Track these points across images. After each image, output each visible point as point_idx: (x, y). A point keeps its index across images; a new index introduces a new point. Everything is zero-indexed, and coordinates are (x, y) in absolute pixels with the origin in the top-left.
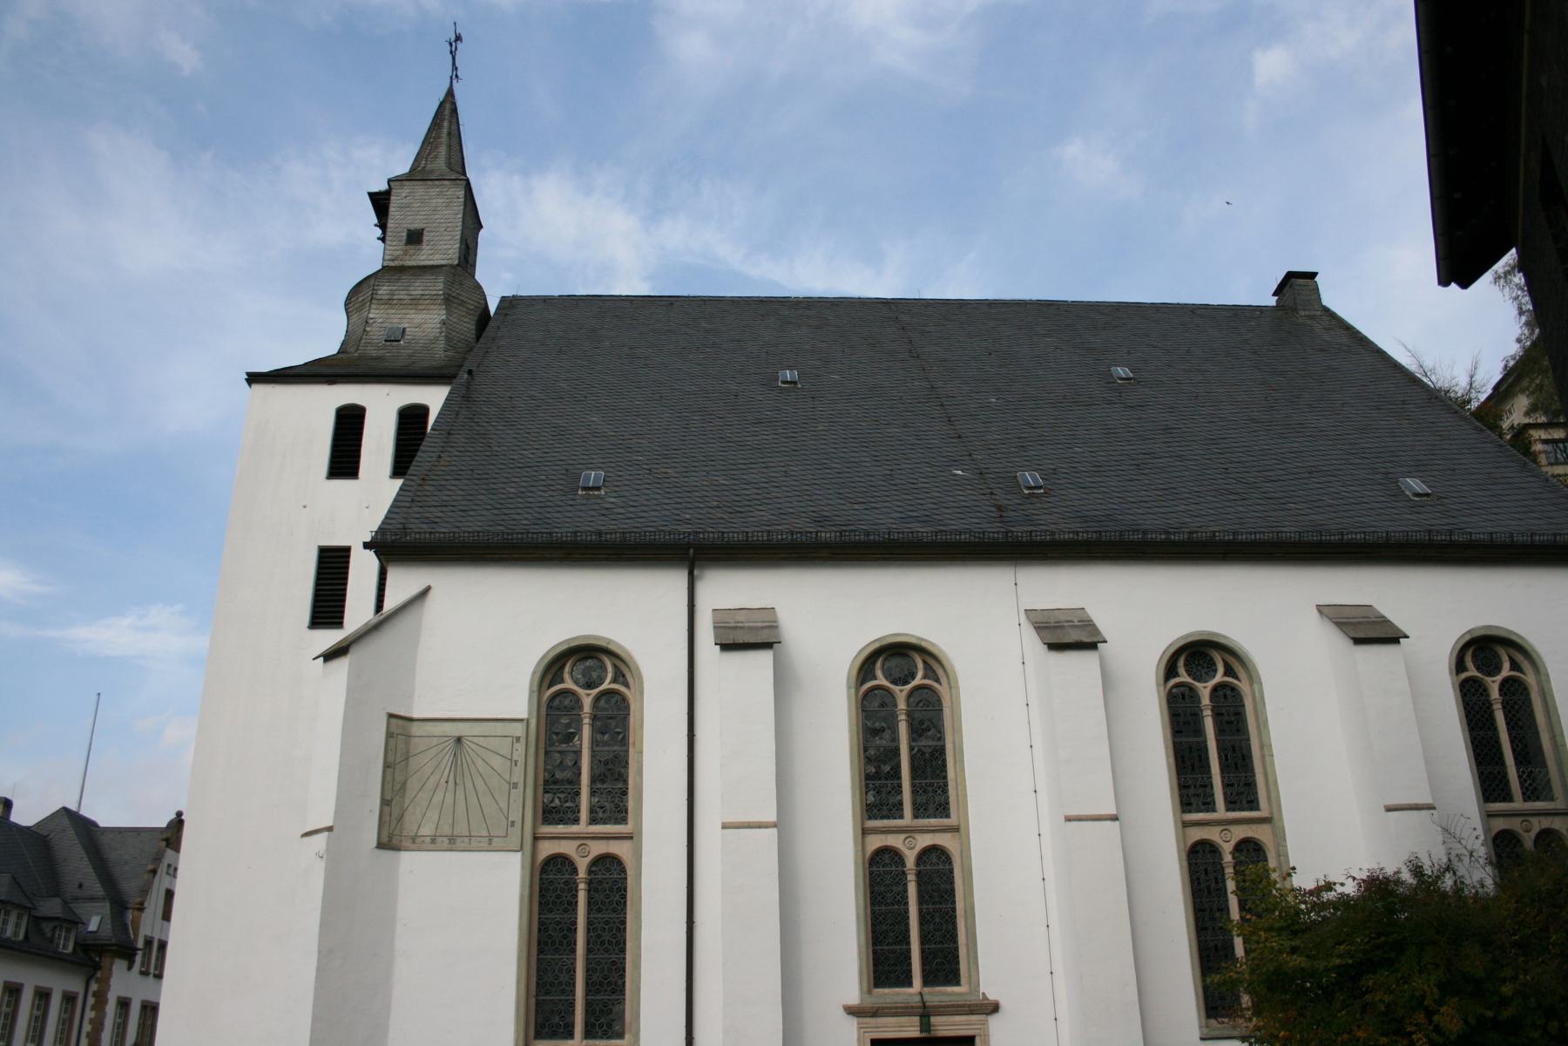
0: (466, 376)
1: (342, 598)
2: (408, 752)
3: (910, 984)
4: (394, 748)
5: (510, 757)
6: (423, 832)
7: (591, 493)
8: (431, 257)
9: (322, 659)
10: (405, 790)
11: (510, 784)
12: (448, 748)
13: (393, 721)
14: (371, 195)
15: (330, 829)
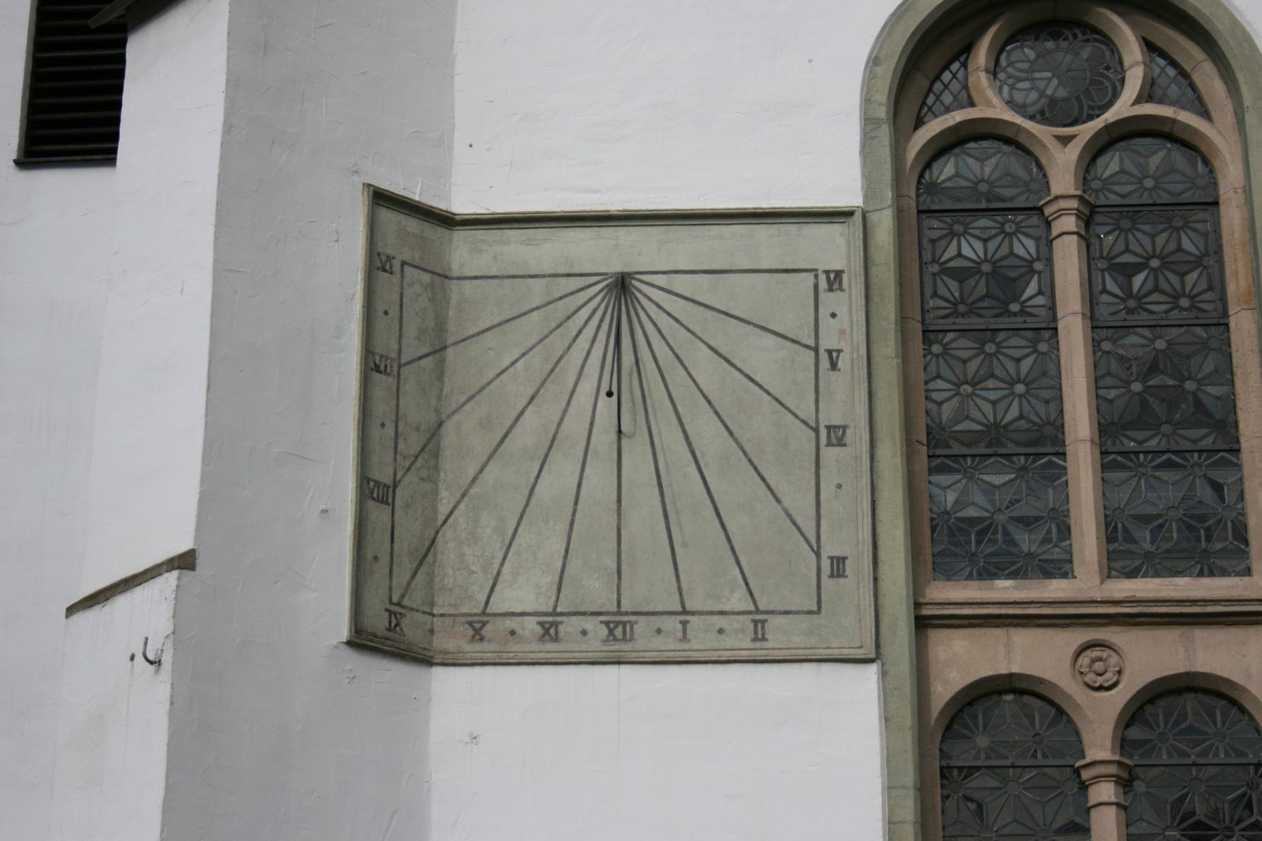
1: (114, 98)
2: (441, 327)
4: (394, 312)
5: (811, 342)
6: (507, 599)
10: (436, 455)
11: (816, 430)
12: (585, 313)
13: (388, 216)
15: (185, 562)
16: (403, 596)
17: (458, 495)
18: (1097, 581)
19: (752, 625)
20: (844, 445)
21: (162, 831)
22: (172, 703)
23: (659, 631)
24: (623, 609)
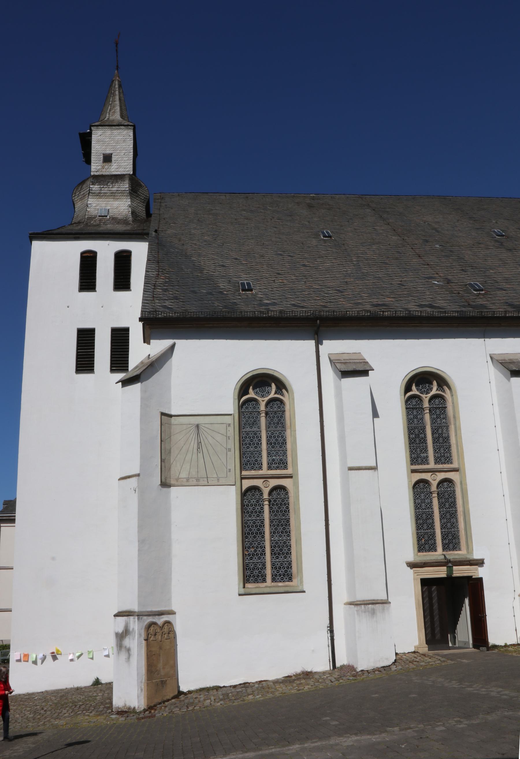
0: (154, 233)
2: (170, 433)
3: (436, 550)
7: (248, 292)
8: (117, 170)
9: (120, 383)
11: (227, 449)
12: (192, 430)
14: (81, 135)
15: (138, 475)
23: (204, 480)
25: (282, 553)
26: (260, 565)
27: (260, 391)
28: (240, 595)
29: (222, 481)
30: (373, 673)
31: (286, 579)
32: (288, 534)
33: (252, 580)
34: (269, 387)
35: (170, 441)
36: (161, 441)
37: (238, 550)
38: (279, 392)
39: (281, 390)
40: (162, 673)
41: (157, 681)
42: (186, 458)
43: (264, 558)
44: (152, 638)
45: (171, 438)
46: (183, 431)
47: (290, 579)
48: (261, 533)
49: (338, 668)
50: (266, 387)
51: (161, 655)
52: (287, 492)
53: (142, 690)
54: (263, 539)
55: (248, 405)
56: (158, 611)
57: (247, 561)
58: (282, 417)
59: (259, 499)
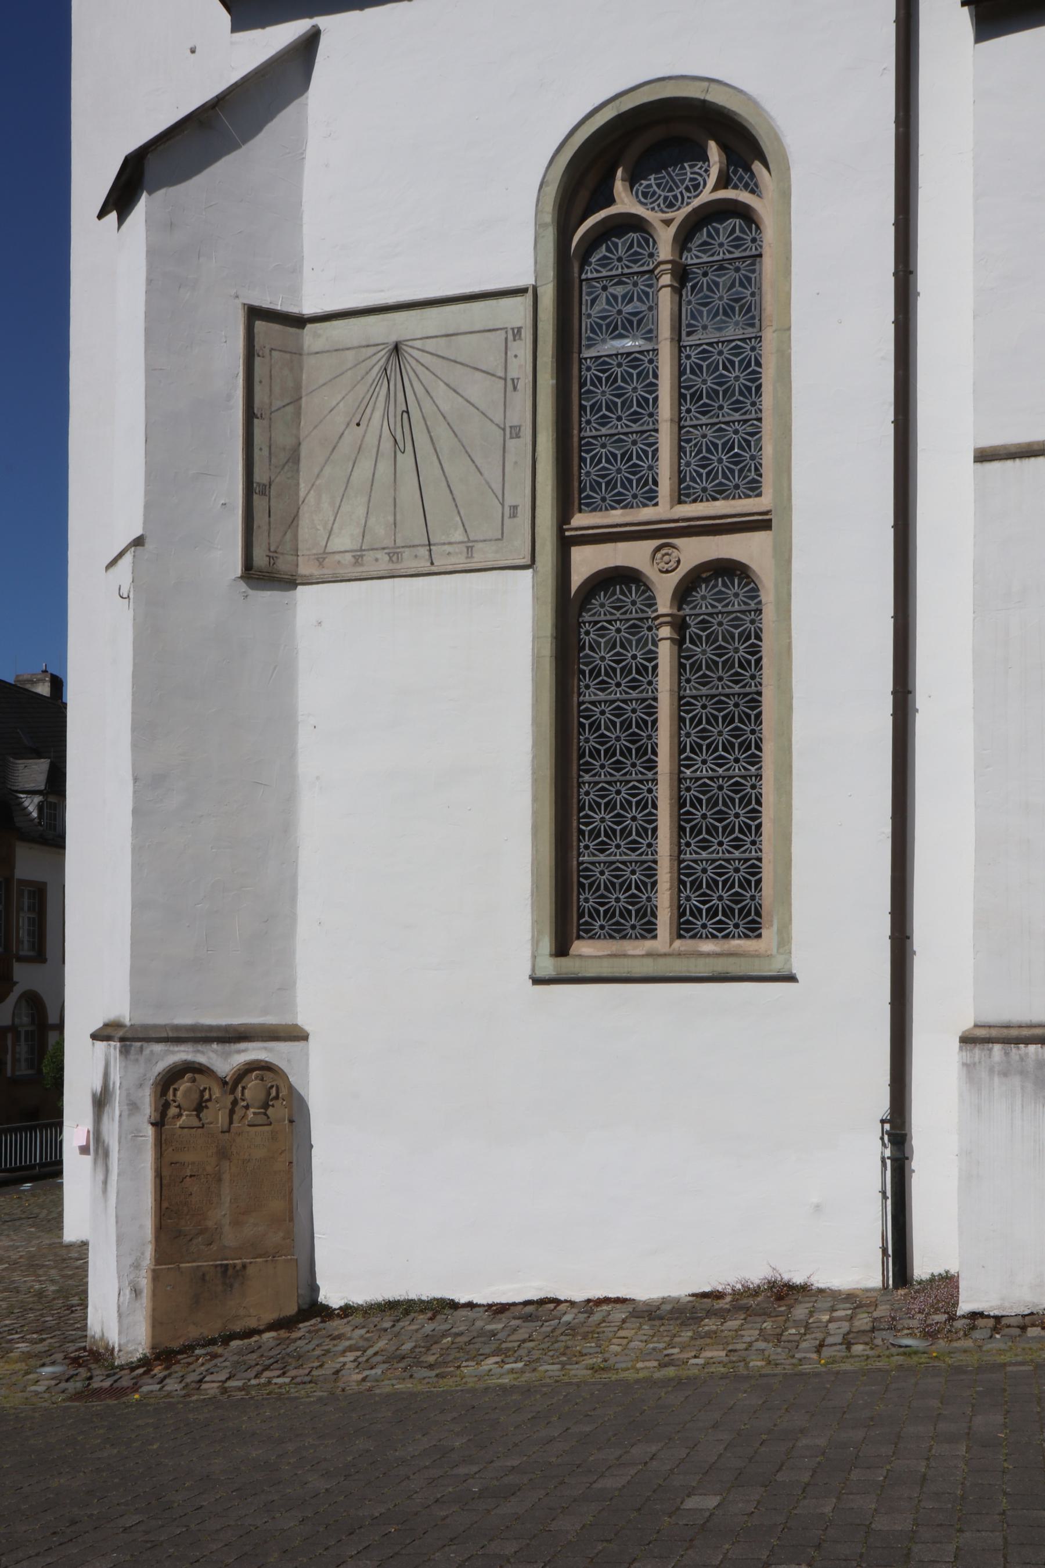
2: (298, 387)
11: (504, 430)
16: (278, 547)
17: (310, 486)
18: (669, 506)
19: (466, 550)
20: (519, 437)
21: (133, 687)
22: (134, 620)
23: (416, 556)
24: (397, 545)
25: (725, 828)
26: (633, 872)
27: (659, 185)
28: (537, 981)
29: (485, 554)
30: (1017, 1331)
31: (736, 926)
32: (754, 757)
33: (602, 927)
34: (700, 164)
35: (298, 414)
36: (250, 415)
37: (535, 814)
38: (741, 179)
39: (748, 169)
40: (230, 1238)
41: (201, 1266)
42: (354, 474)
43: (650, 845)
44: (184, 1118)
45: (300, 407)
46: (343, 373)
47: (754, 930)
48: (641, 752)
49: (920, 1283)
50: (686, 165)
51: (226, 1177)
52: (756, 589)
53: (136, 1292)
54: (650, 775)
55: (608, 250)
56: (227, 1028)
57: (586, 858)
58: (746, 282)
59: (641, 619)
